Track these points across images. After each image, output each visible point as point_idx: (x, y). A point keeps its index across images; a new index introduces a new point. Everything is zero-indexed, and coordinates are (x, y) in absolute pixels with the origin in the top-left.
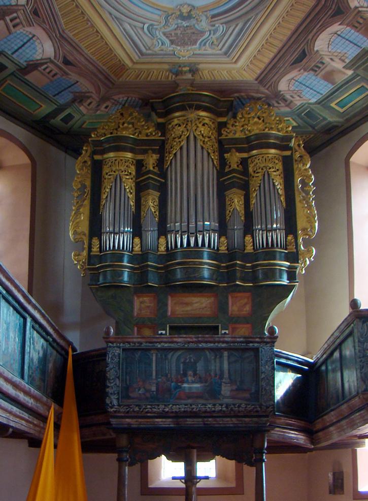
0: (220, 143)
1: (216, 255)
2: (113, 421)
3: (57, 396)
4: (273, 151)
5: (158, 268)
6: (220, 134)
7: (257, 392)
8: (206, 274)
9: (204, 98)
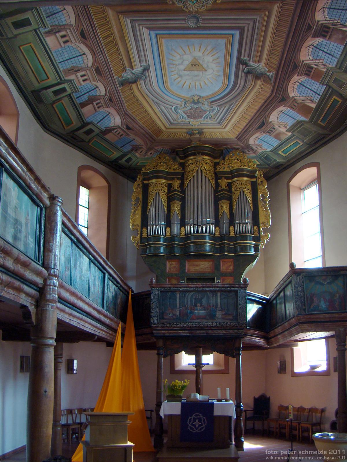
0: (216, 174)
1: (213, 238)
2: (155, 332)
3: (123, 318)
4: (246, 178)
6: (215, 169)
7: (237, 315)
8: (208, 248)
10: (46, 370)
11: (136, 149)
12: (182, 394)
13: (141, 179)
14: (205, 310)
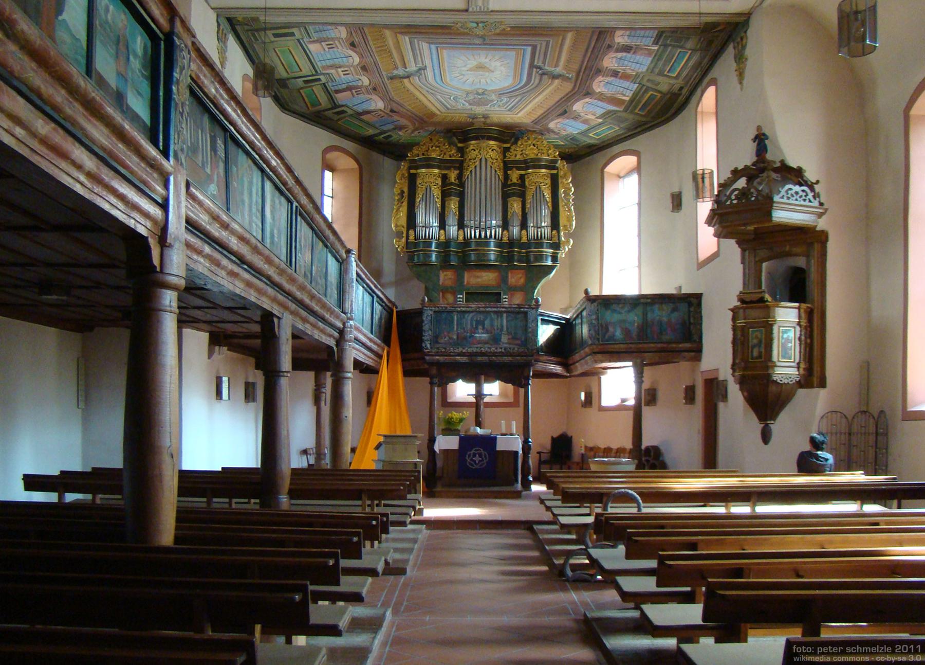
0: (505, 163)
1: (500, 244)
2: (427, 358)
3: (386, 340)
4: (543, 170)
5: (458, 252)
6: (505, 157)
7: (526, 340)
8: (492, 257)
9: (492, 131)
10: (346, 398)
11: (401, 128)
12: (459, 428)
13: (406, 166)
14: (488, 333)
